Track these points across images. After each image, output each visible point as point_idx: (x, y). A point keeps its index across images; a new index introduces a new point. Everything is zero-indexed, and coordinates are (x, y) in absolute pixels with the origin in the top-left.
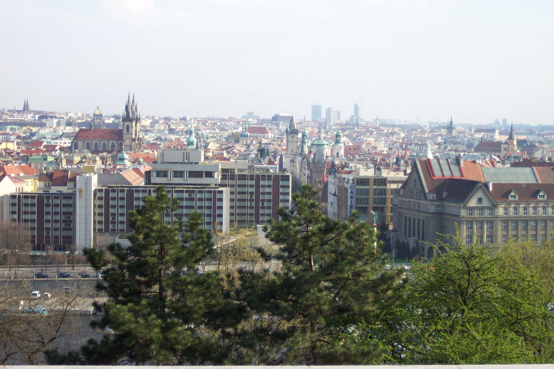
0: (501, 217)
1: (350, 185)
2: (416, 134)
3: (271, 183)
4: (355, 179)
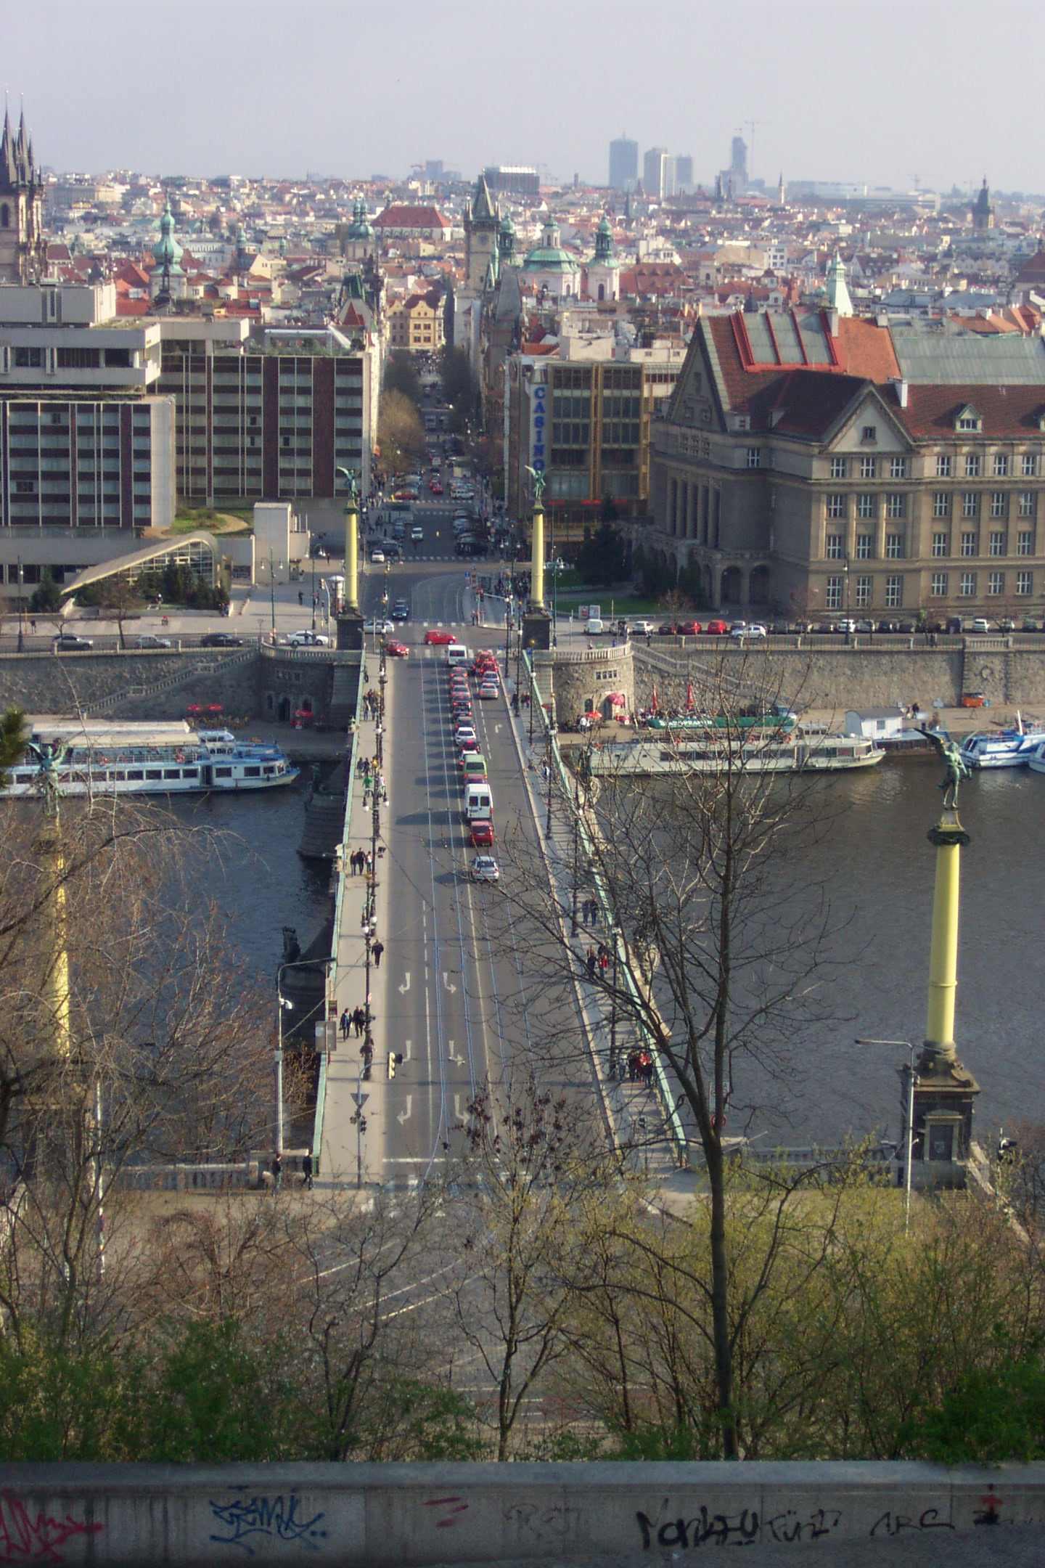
0: (931, 483)
1: (534, 387)
2: (883, 228)
3: (310, 381)
4: (550, 370)
